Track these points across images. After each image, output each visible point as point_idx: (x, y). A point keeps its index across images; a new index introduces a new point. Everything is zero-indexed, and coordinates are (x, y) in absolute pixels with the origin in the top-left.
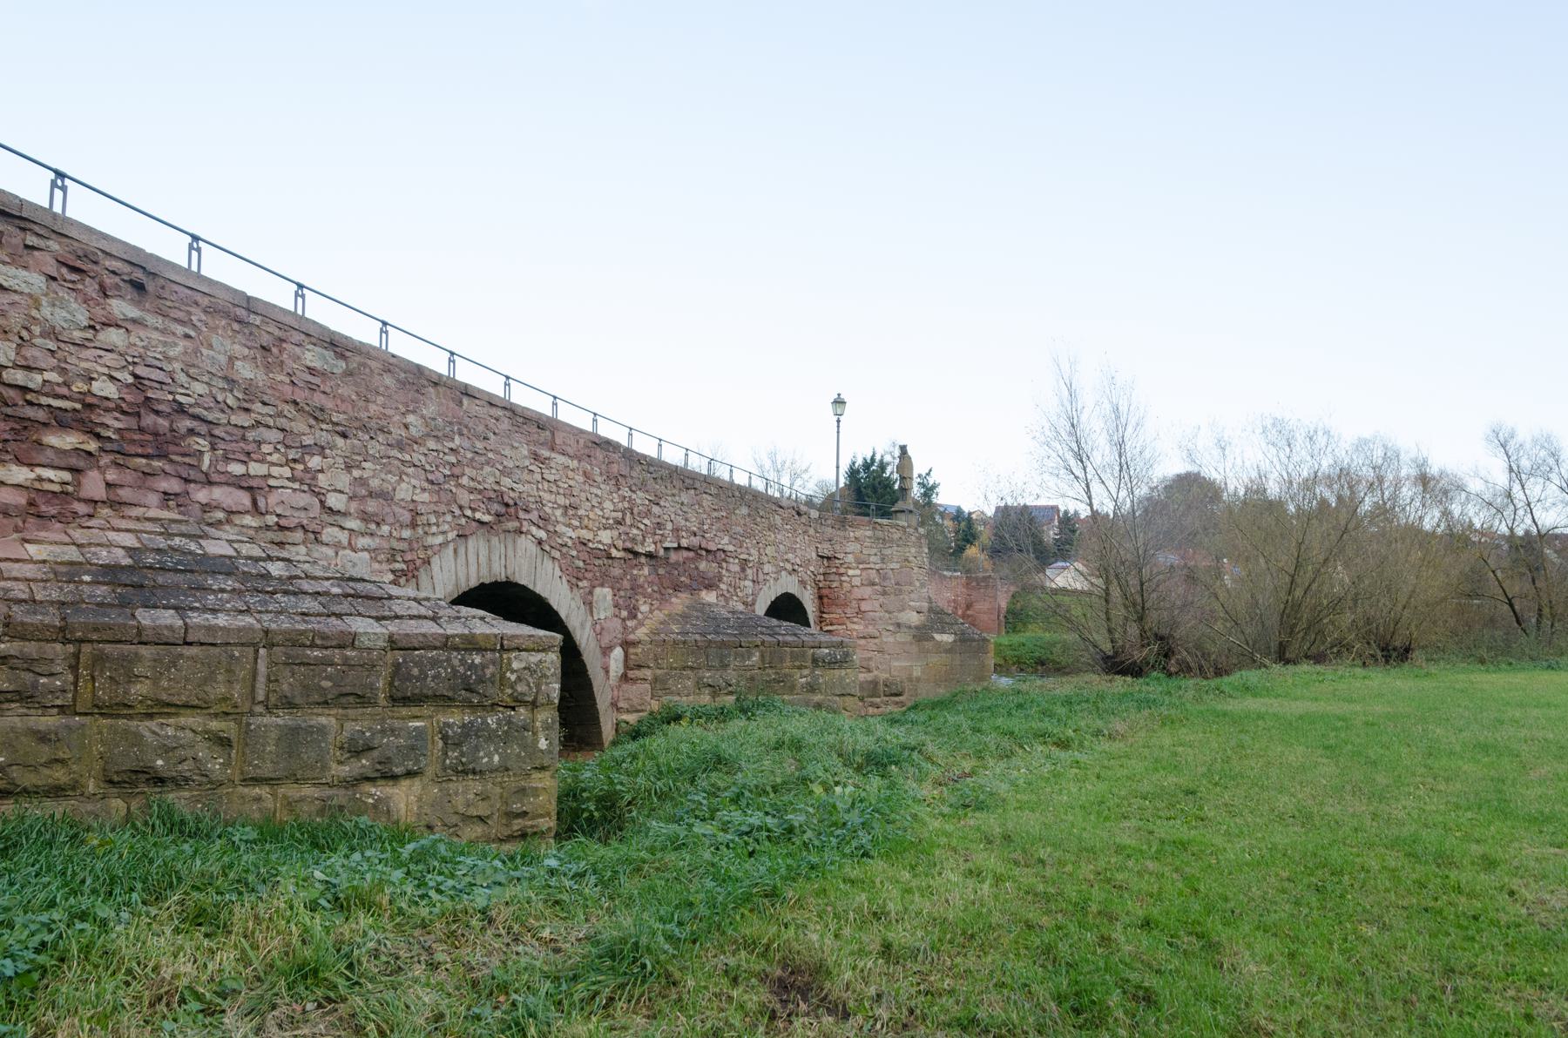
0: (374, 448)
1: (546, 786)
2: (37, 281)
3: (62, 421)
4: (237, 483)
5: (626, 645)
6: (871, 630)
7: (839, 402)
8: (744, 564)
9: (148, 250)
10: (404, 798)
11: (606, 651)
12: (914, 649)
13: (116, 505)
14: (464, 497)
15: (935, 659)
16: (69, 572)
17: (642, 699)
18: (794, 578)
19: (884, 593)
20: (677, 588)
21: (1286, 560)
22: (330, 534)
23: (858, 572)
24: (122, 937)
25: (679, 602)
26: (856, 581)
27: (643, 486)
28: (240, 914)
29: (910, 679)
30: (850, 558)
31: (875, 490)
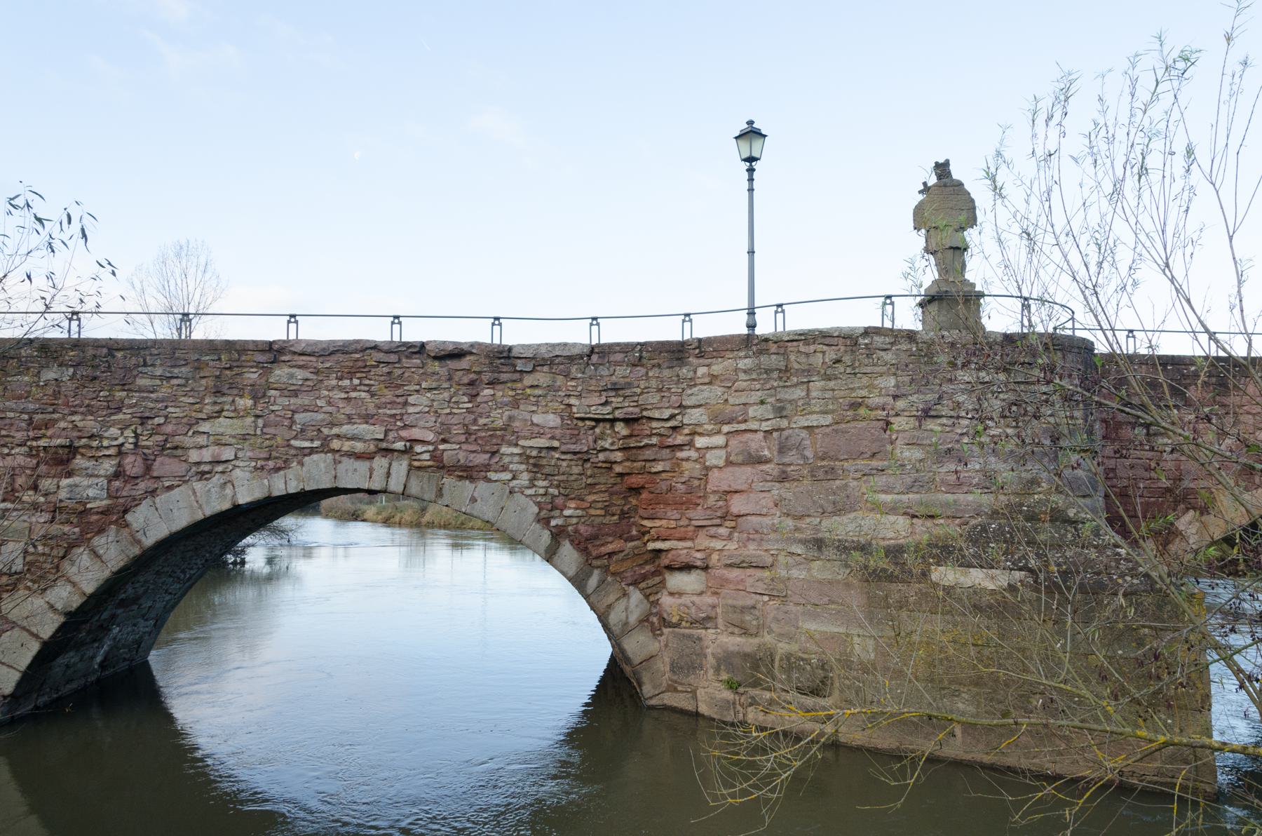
7: (751, 133)
12: (855, 600)
15: (927, 627)
19: (783, 478)
23: (719, 440)
29: (846, 663)
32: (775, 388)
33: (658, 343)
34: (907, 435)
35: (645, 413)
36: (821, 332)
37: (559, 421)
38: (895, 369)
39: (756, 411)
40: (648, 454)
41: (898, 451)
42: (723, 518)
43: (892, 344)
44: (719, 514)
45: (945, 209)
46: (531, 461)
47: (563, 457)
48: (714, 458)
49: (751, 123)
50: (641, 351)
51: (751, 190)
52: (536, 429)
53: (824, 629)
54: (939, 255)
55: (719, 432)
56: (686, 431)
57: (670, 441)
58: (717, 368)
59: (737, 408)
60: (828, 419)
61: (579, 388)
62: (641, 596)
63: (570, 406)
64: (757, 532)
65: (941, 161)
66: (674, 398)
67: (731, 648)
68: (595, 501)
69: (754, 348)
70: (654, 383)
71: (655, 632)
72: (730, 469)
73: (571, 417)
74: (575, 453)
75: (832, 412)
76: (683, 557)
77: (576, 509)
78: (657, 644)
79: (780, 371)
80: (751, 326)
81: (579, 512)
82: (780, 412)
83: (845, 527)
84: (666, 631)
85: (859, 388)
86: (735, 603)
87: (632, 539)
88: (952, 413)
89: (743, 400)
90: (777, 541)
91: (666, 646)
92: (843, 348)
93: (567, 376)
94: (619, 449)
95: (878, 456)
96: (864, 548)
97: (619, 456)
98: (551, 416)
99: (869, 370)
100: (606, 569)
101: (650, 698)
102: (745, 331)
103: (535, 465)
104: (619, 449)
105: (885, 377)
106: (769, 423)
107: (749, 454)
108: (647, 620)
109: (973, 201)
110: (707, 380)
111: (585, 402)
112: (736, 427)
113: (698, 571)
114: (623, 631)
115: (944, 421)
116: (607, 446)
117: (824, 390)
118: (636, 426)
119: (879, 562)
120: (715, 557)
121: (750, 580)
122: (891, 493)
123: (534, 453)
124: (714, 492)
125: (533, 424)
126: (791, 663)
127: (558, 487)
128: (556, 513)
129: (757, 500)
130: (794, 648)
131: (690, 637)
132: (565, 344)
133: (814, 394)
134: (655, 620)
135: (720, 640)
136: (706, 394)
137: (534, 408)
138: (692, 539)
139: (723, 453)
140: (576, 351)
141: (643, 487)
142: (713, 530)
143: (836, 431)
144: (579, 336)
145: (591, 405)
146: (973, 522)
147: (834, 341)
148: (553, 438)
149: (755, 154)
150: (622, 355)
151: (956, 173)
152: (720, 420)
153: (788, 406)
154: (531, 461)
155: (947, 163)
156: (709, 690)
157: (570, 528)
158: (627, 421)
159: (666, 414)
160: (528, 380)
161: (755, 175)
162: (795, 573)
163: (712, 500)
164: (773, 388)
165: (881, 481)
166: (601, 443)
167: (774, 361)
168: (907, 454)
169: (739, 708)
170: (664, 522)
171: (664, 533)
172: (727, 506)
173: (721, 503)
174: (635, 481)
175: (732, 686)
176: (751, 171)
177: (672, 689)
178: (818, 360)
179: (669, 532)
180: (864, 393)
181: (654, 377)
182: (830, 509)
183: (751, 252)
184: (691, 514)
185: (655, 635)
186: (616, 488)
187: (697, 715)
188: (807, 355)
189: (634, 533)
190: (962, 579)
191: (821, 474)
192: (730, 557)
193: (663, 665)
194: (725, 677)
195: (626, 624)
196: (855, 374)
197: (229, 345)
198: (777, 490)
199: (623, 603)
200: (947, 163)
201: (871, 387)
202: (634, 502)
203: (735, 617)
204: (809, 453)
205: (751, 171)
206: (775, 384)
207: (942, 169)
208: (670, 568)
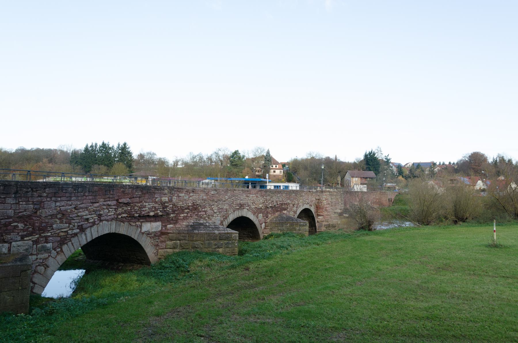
0: (220, 203)
1: (237, 249)
2: (184, 194)
3: (186, 209)
4: (204, 211)
5: (265, 223)
8: (293, 205)
10: (221, 250)
11: (261, 224)
12: (339, 218)
13: (191, 216)
14: (234, 206)
15: (344, 220)
16: (187, 226)
17: (267, 232)
18: (308, 205)
20: (277, 211)
21: (418, 201)
22: (215, 215)
24: (195, 262)
25: (277, 214)
26: (325, 204)
27: (269, 195)
28: (204, 260)
30: (324, 199)
31: (372, 160)
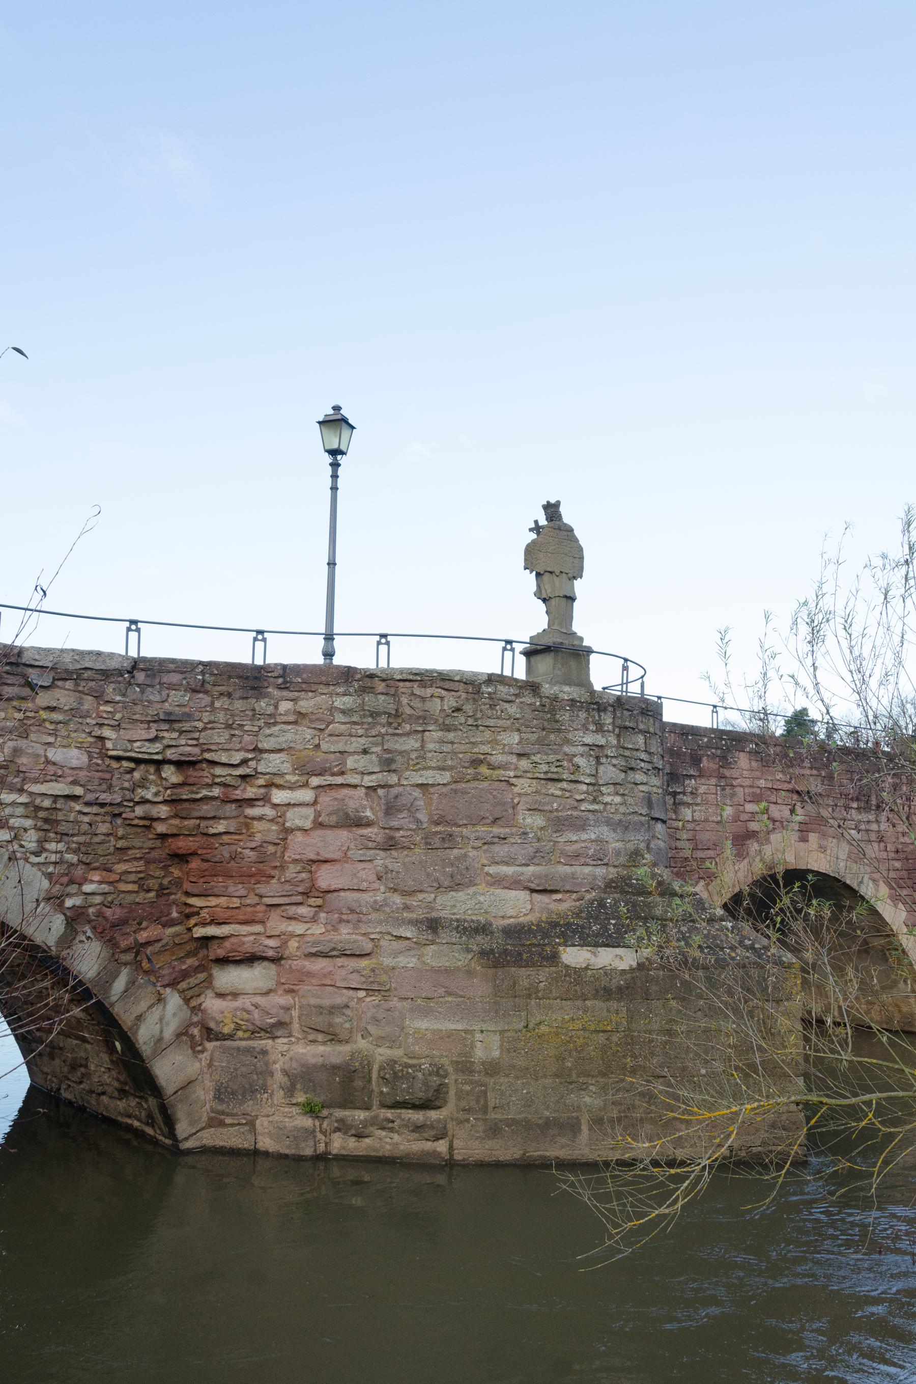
6: (345, 935)
7: (336, 422)
9: (590, 666)
12: (479, 989)
15: (558, 1016)
19: (390, 845)
23: (306, 795)
29: (465, 1067)
32: (382, 736)
33: (228, 665)
34: (529, 799)
35: (207, 756)
36: (440, 673)
37: (85, 759)
38: (518, 725)
39: (356, 761)
40: (206, 809)
41: (521, 817)
42: (305, 894)
43: (516, 695)
44: (301, 889)
45: (554, 554)
46: (41, 814)
47: (86, 810)
48: (297, 818)
49: (337, 409)
50: (203, 673)
51: (334, 489)
52: (51, 769)
53: (437, 1026)
54: (553, 602)
55: (306, 785)
56: (261, 782)
57: (238, 794)
58: (305, 705)
59: (332, 756)
60: (446, 777)
61: (118, 716)
62: (181, 1001)
63: (101, 739)
64: (352, 911)
65: (553, 501)
66: (247, 738)
67: (312, 1061)
68: (127, 872)
69: (356, 685)
70: (221, 717)
71: (195, 1048)
72: (319, 832)
73: (103, 755)
74: (102, 805)
75: (451, 768)
76: (248, 945)
77: (100, 882)
78: (197, 1065)
79: (390, 715)
80: (328, 654)
81: (105, 888)
82: (388, 764)
83: (459, 904)
84: (209, 1045)
85: (482, 743)
86: (319, 1002)
87: (172, 923)
88: (572, 777)
89: (340, 747)
90: (380, 922)
91: (210, 1065)
92: (464, 695)
93: (99, 697)
94: (165, 802)
95: (500, 822)
96: (482, 929)
97: (163, 811)
98: (74, 752)
99: (491, 722)
100: (136, 964)
101: (186, 1139)
102: (320, 660)
103: (46, 821)
104: (165, 802)
105: (508, 733)
106: (374, 777)
107: (347, 814)
108: (185, 1033)
109: (580, 549)
110: (291, 718)
111: (125, 734)
112: (330, 780)
113: (266, 963)
114: (155, 1050)
115: (564, 785)
116: (149, 796)
117: (442, 742)
118: (191, 772)
119: (496, 942)
120: (293, 944)
121: (343, 972)
122: (513, 864)
123: (47, 803)
124: (295, 861)
125: (48, 762)
126: (394, 1073)
127: (75, 851)
128: (73, 889)
129: (354, 871)
130: (397, 1053)
131: (248, 1051)
132: (99, 654)
133: (430, 746)
134: (196, 1031)
135: (293, 1051)
136: (289, 736)
137: (51, 739)
138: (262, 922)
139: (310, 812)
140: (113, 664)
141: (194, 854)
142: (292, 910)
143: (456, 791)
144: (110, 641)
145: (138, 740)
146: (588, 897)
147: (455, 686)
148: (75, 783)
149: (343, 448)
150: (180, 676)
151: (568, 516)
152: (306, 770)
153: (399, 759)
154: (41, 814)
155: (558, 504)
156: (276, 1118)
157: (91, 910)
158: (179, 764)
159: (237, 758)
160: (43, 699)
161: (340, 471)
162: (402, 961)
163: (291, 871)
164: (380, 735)
165: (500, 850)
166: (141, 793)
167: (381, 702)
168: (529, 820)
169: (319, 1136)
170: (222, 901)
171: (220, 914)
172: (312, 880)
173: (304, 875)
174: (183, 845)
175: (310, 1110)
176: (335, 465)
177: (216, 1122)
178: (435, 706)
179: (230, 913)
180: (486, 749)
181: (222, 709)
182: (446, 883)
183: (332, 564)
184: (262, 889)
185: (195, 1052)
186: (154, 854)
187: (255, 1153)
188: (423, 699)
189: (175, 915)
190: (593, 960)
191: (436, 842)
192: (315, 943)
193: (204, 1094)
194: (301, 1098)
195: (160, 1040)
196: (477, 726)
197: (442, 680)
198: (381, 860)
199: (156, 1012)
200: (558, 504)
201: (494, 742)
202: (176, 873)
203: (320, 1021)
204: (422, 816)
205: (335, 465)
206: (383, 731)
207: (552, 510)
208: (224, 961)
